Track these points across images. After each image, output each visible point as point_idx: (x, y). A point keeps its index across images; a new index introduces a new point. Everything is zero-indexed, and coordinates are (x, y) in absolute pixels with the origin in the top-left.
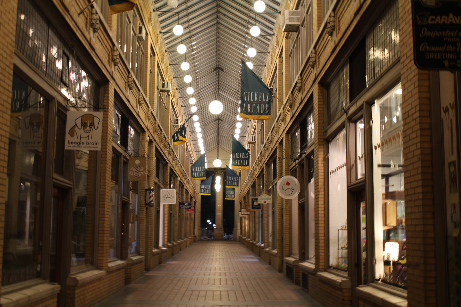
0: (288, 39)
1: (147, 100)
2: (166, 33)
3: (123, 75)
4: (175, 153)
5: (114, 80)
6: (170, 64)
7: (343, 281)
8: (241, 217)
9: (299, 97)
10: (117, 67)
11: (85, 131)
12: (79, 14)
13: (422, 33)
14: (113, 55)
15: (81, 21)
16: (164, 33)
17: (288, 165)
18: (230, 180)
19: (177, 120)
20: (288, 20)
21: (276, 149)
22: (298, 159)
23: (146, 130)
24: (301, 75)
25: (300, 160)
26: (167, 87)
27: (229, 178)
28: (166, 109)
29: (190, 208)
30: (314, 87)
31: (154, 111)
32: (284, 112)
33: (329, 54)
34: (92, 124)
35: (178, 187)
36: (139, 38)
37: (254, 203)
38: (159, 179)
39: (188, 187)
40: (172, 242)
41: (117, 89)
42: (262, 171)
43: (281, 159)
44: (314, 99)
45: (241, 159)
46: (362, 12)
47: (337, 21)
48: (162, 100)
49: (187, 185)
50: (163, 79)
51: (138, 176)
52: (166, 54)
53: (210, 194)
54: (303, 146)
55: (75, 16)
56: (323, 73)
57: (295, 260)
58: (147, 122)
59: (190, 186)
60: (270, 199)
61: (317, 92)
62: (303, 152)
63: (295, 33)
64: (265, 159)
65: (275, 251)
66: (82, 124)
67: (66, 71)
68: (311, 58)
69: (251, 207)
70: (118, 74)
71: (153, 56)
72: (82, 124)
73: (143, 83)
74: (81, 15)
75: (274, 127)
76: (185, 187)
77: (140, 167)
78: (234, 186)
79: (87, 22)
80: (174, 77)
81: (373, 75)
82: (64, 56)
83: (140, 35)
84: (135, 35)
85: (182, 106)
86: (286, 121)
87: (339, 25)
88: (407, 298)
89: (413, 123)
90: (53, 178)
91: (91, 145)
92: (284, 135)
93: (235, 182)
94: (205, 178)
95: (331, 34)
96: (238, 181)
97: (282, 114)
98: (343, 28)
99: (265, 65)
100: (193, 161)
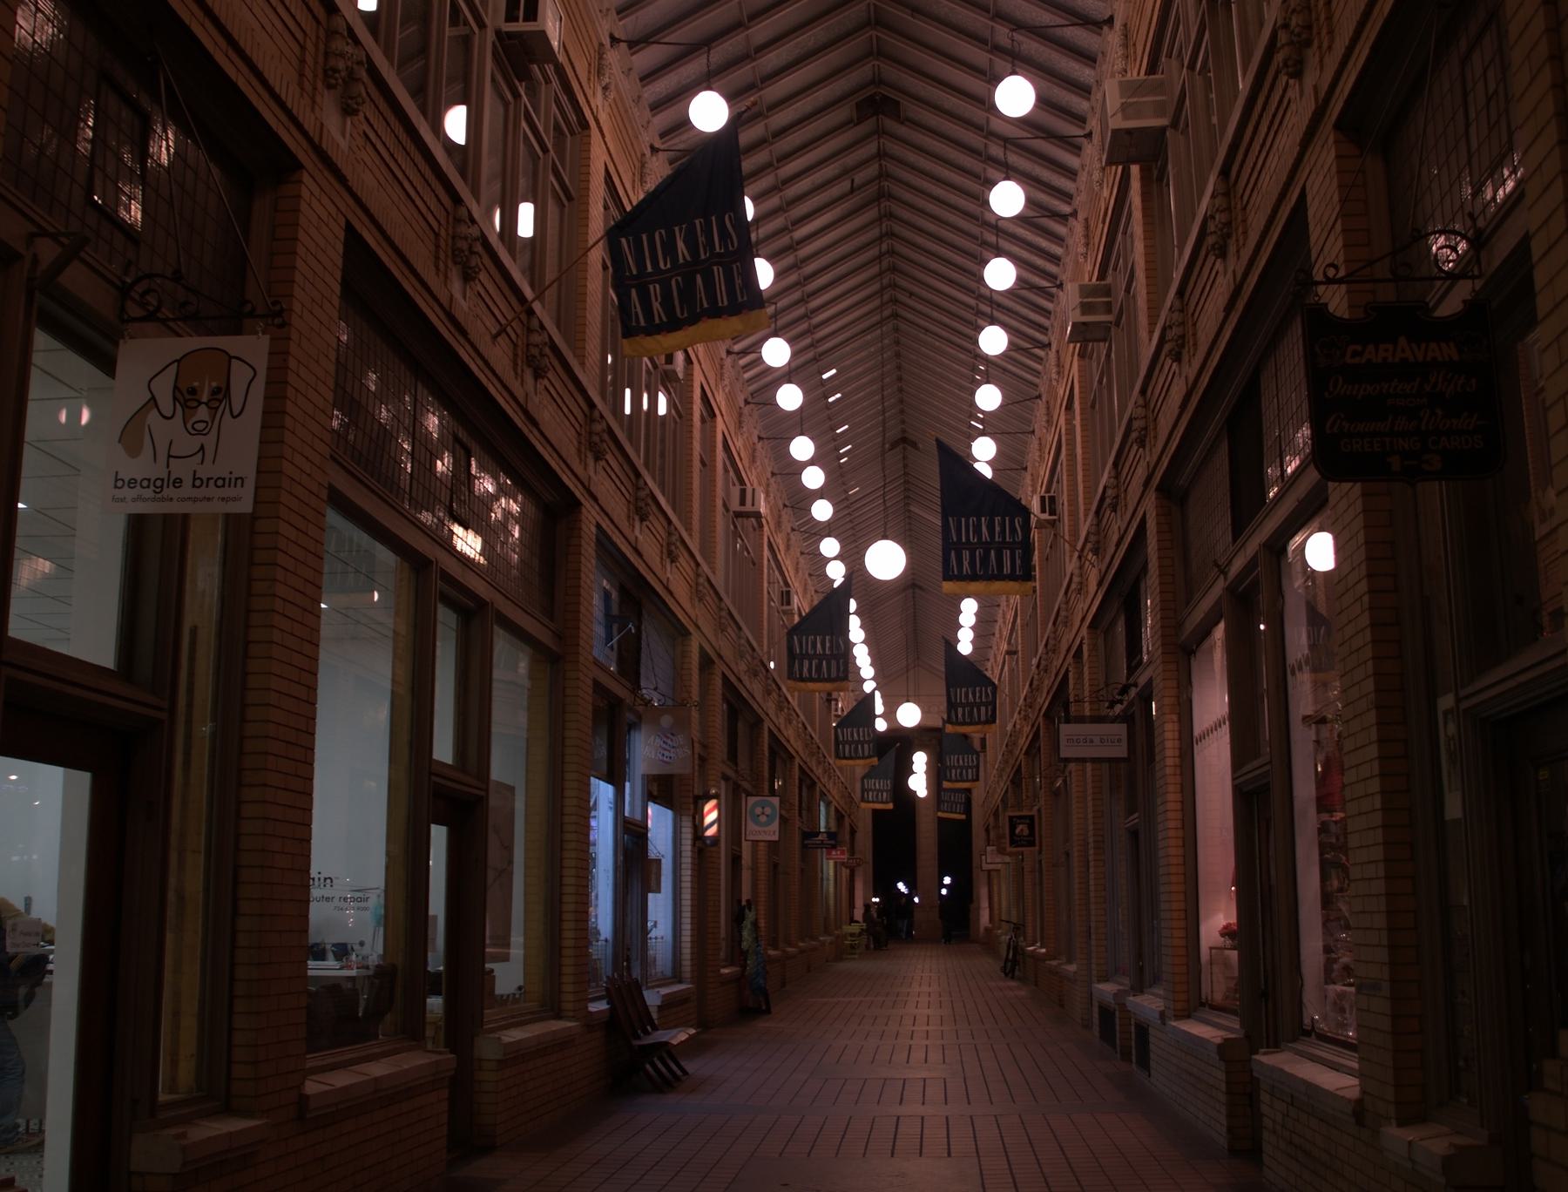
0: (1087, 360)
2: (744, 352)
3: (622, 483)
5: (595, 499)
6: (760, 438)
7: (1226, 1040)
8: (989, 871)
9: (1116, 525)
10: (603, 463)
11: (189, 426)
12: (495, 337)
14: (591, 433)
15: (499, 355)
16: (738, 353)
19: (788, 593)
20: (1078, 311)
22: (1121, 702)
23: (692, 629)
24: (1115, 464)
26: (753, 505)
27: (952, 760)
28: (754, 564)
31: (714, 573)
32: (1081, 567)
33: (1177, 411)
34: (221, 394)
35: (797, 791)
36: (667, 376)
37: (1015, 828)
38: (736, 764)
39: (830, 786)
41: (605, 524)
42: (1036, 736)
46: (1240, 305)
47: (1190, 323)
49: (824, 780)
50: (742, 482)
51: (668, 760)
52: (746, 410)
53: (890, 806)
55: (485, 345)
57: (1119, 990)
58: (693, 606)
59: (835, 783)
62: (1131, 681)
63: (1102, 344)
64: (1043, 700)
65: (1072, 968)
66: (178, 395)
67: (462, 477)
68: (1135, 419)
69: (1008, 840)
70: (608, 483)
71: (708, 419)
72: (178, 395)
73: (680, 499)
74: (502, 340)
77: (672, 734)
79: (516, 355)
80: (776, 471)
82: (457, 446)
83: (668, 367)
84: (655, 366)
85: (802, 553)
88: (1359, 1074)
90: (431, 774)
91: (211, 491)
92: (1084, 632)
93: (970, 771)
94: (875, 760)
95: (1178, 358)
97: (1077, 572)
98: (1204, 339)
99: (1031, 429)
100: (843, 710)
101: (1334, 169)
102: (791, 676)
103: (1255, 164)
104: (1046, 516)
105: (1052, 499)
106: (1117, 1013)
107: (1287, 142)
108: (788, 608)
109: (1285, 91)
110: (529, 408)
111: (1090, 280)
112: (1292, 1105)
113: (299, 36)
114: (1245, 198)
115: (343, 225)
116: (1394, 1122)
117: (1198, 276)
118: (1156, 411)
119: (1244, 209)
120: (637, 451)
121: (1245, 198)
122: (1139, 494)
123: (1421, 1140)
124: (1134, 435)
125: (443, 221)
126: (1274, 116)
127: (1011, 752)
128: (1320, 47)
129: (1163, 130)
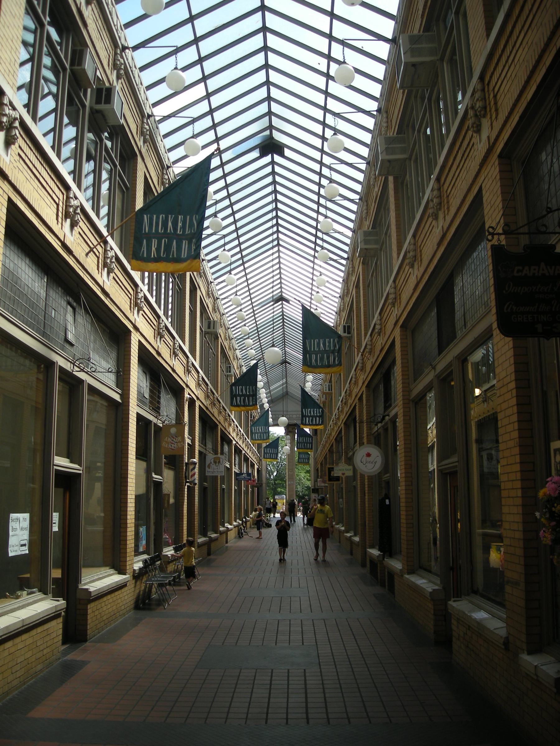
1: (186, 349)
4: (227, 410)
7: (434, 590)
12: (87, 254)
13: (507, 289)
15: (91, 263)
17: (370, 429)
18: (301, 442)
19: (230, 367)
21: (355, 406)
22: (381, 422)
25: (383, 423)
26: (214, 328)
29: (250, 479)
30: (396, 332)
32: (363, 359)
33: (411, 291)
40: (226, 524)
42: (340, 432)
43: (361, 422)
44: (396, 347)
45: (313, 417)
46: (446, 243)
48: (209, 344)
51: (174, 448)
54: (387, 405)
56: (405, 314)
60: (350, 470)
61: (399, 338)
62: (386, 413)
65: (357, 539)
75: (352, 377)
76: (243, 452)
77: (176, 437)
78: (307, 449)
81: (463, 323)
86: (365, 371)
87: (421, 256)
89: (508, 396)
90: (54, 465)
92: (364, 388)
95: (412, 266)
96: (312, 443)
97: (361, 361)
101: (498, 177)
102: (232, 405)
103: (454, 175)
104: (346, 335)
105: (349, 327)
106: (379, 565)
107: (473, 165)
108: (230, 373)
109: (471, 139)
110: (105, 288)
111: (368, 229)
112: (469, 629)
113: (130, 296)
114: (449, 191)
115: (7, 199)
116: (526, 652)
117: (423, 228)
118: (401, 290)
119: (448, 196)
120: (160, 307)
121: (449, 191)
122: (392, 328)
123: (542, 665)
124: (390, 301)
125: (132, 294)
126: (465, 152)
127: (329, 437)
128: (491, 118)
129: (404, 160)
